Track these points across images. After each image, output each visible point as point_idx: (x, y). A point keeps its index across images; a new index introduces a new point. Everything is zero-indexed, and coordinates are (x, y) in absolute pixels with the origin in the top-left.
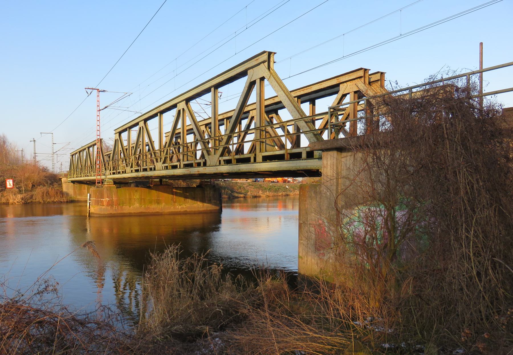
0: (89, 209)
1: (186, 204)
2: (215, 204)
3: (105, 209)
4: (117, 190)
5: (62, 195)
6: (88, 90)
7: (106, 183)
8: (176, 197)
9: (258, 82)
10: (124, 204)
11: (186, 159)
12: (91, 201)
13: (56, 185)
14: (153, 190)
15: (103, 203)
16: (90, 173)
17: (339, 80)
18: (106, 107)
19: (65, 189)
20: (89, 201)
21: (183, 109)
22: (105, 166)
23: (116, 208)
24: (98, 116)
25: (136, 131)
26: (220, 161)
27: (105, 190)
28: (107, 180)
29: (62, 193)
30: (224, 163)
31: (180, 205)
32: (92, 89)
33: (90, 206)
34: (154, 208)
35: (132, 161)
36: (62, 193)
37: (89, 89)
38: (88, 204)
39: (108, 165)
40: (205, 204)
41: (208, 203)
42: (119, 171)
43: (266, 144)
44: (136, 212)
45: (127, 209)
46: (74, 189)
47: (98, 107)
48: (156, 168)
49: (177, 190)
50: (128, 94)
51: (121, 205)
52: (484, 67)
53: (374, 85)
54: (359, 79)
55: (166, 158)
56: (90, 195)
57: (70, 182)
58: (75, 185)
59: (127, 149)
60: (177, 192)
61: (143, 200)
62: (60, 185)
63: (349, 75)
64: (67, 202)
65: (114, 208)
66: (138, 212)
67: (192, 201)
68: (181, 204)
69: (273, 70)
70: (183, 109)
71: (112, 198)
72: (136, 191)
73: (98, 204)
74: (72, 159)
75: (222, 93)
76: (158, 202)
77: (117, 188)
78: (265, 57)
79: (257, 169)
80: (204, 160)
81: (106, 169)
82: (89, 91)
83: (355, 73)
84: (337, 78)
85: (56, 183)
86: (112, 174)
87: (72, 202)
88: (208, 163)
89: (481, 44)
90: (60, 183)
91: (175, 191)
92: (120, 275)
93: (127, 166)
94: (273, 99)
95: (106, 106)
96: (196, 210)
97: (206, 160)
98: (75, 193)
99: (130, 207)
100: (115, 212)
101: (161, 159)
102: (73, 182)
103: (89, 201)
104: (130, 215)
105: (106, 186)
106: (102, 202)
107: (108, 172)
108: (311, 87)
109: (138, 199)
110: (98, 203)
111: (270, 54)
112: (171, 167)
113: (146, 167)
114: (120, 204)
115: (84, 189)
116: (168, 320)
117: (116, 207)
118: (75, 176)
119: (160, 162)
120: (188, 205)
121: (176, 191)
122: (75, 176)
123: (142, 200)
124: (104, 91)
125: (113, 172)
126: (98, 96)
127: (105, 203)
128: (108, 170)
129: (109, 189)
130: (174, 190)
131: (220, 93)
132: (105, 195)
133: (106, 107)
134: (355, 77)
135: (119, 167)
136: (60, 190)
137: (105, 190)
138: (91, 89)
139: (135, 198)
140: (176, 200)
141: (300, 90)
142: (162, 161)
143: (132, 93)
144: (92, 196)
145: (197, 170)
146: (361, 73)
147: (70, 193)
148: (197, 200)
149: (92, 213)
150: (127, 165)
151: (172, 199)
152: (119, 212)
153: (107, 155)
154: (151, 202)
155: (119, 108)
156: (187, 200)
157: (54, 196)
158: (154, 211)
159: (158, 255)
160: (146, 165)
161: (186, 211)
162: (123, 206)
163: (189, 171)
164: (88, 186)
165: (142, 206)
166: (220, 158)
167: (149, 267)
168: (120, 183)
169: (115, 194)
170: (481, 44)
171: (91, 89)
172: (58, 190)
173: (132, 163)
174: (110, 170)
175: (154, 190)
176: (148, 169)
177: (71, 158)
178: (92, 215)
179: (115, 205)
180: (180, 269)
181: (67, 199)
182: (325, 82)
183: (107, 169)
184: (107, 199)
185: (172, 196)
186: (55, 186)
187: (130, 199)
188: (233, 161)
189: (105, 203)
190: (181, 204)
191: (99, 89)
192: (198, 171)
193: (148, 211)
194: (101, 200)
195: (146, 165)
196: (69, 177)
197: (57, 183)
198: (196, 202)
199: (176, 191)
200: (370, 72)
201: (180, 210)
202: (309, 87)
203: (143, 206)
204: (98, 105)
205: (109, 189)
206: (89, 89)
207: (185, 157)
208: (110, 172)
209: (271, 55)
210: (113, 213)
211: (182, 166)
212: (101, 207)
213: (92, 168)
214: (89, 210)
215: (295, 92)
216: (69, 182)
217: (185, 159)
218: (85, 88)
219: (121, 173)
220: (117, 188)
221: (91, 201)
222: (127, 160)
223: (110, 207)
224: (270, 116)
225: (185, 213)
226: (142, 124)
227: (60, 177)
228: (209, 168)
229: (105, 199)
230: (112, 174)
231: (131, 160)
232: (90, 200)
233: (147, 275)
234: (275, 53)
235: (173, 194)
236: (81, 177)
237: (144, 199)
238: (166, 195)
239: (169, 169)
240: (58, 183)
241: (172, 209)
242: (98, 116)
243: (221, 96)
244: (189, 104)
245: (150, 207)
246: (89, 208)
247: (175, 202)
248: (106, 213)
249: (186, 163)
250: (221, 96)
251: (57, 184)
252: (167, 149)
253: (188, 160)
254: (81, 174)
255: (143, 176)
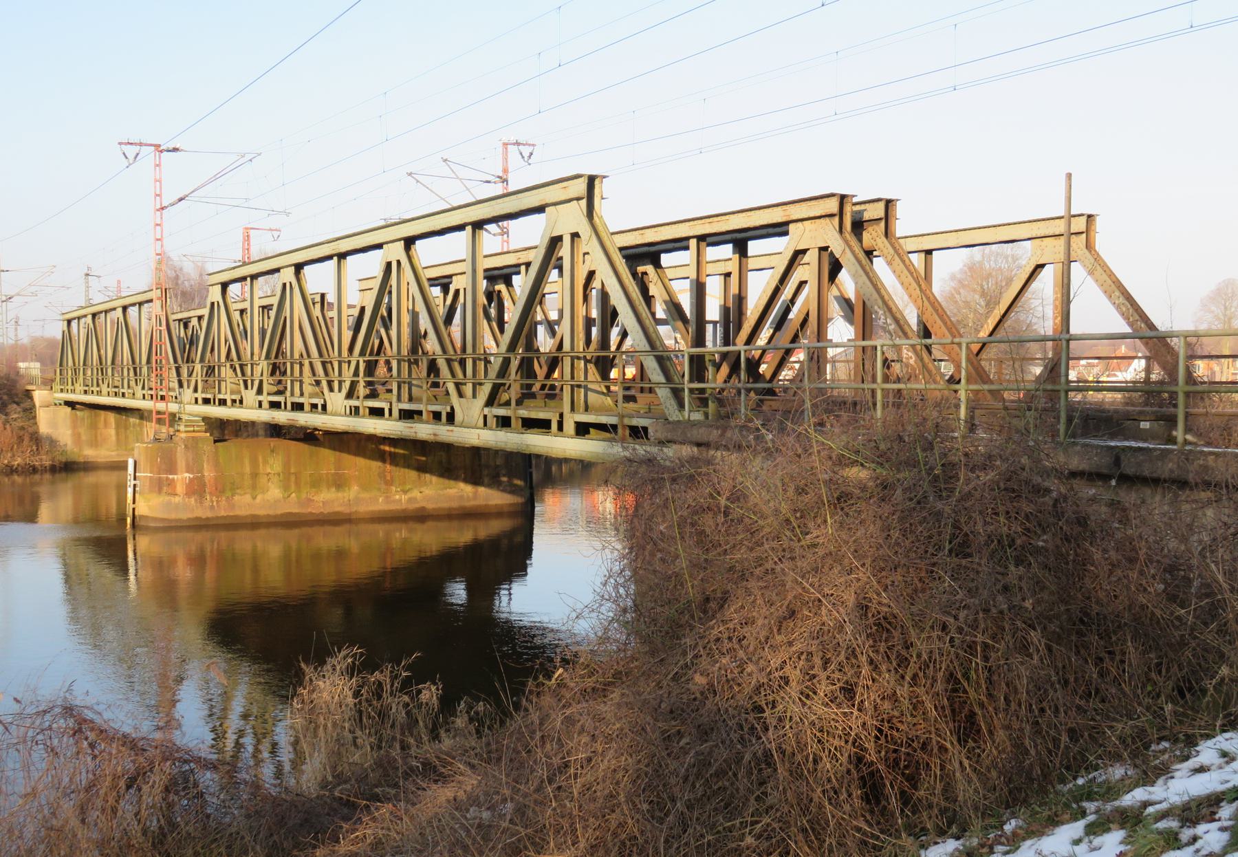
0: (132, 506)
1: (422, 489)
2: (513, 490)
3: (180, 505)
4: (216, 448)
5: (37, 446)
6: (127, 149)
7: (182, 428)
8: (394, 468)
9: (567, 240)
10: (238, 491)
11: (407, 395)
12: (137, 482)
13: (15, 412)
14: (322, 449)
15: (175, 487)
16: (129, 387)
17: (787, 213)
18: (181, 200)
19: (44, 428)
20: (133, 482)
21: (399, 262)
22: (179, 374)
23: (212, 502)
24: (157, 225)
25: (271, 230)
26: (485, 417)
27: (180, 449)
28: (185, 417)
29: (36, 439)
30: (497, 426)
31: (405, 492)
32: (141, 144)
33: (137, 495)
34: (327, 500)
35: (262, 375)
36: (37, 439)
37: (131, 144)
38: (130, 490)
39: (190, 375)
40: (482, 490)
41: (489, 486)
42: (221, 396)
43: (586, 389)
44: (271, 512)
45: (245, 504)
46: (74, 425)
47: (158, 198)
48: (329, 407)
49: (395, 447)
50: (248, 157)
51: (229, 494)
52: (1061, 241)
53: (870, 229)
54: (828, 220)
55: (353, 385)
56: (135, 463)
57: (62, 403)
58: (78, 413)
59: (242, 312)
60: (395, 453)
61: (293, 478)
62: (30, 412)
63: (809, 203)
64: (54, 469)
65: (207, 503)
66: (279, 512)
67: (441, 480)
68: (408, 487)
69: (601, 218)
70: (399, 262)
71: (201, 471)
72: (272, 451)
73: (160, 491)
74: (66, 332)
75: (533, 145)
76: (339, 483)
77: (215, 441)
78: (580, 187)
79: (564, 450)
80: (449, 409)
81: (181, 385)
82: (131, 151)
83: (821, 201)
84: (784, 207)
85: (15, 406)
86: (200, 401)
87: (68, 468)
88: (459, 417)
89: (1069, 176)
90: (27, 404)
91: (390, 452)
92: (226, 697)
93: (246, 388)
94: (641, 232)
95: (181, 196)
96: (455, 504)
97: (452, 408)
98: (77, 437)
99: (254, 498)
100: (209, 514)
101: (340, 383)
102: (71, 404)
103: (133, 482)
104: (254, 524)
105: (183, 435)
106: (171, 483)
107: (188, 394)
108: (727, 217)
109: (279, 474)
110: (160, 486)
111: (591, 180)
112: (367, 410)
113: (301, 400)
114: (223, 491)
115: (106, 424)
116: (330, 779)
117: (214, 498)
118: (79, 387)
119: (340, 390)
120: (428, 491)
121: (392, 450)
122: (79, 387)
123: (289, 480)
124: (175, 150)
125: (204, 396)
126: (157, 165)
127: (180, 489)
128: (188, 387)
129: (192, 444)
130: (387, 448)
131: (530, 145)
132: (181, 462)
133: (181, 200)
134: (818, 214)
135: (223, 384)
136: (31, 430)
137: (180, 449)
138: (135, 144)
139: (269, 470)
140: (392, 478)
141: (703, 221)
142: (345, 391)
143: (259, 154)
144: (141, 465)
145: (431, 432)
146: (832, 206)
147: (60, 438)
148: (456, 478)
149: (141, 517)
150: (245, 382)
151: (382, 475)
152: (223, 513)
153: (180, 320)
154: (316, 483)
155: (203, 200)
156: (428, 476)
157: (12, 449)
158: (327, 510)
159: (316, 668)
160: (302, 394)
161: (423, 509)
162: (233, 495)
163: (413, 430)
164: (118, 416)
165: (289, 496)
166: (486, 411)
167: (300, 690)
168: (223, 430)
169: (208, 461)
170: (1069, 176)
171: (135, 144)
172: (22, 428)
173: (261, 382)
174: (196, 390)
175: (324, 447)
176: (307, 407)
177: (66, 328)
178: (142, 523)
179: (211, 494)
180: (357, 694)
181: (53, 460)
182: (757, 212)
183: (185, 385)
184: (187, 475)
185: (380, 464)
186: (15, 416)
187: (255, 475)
188: (513, 421)
189: (180, 489)
190: (408, 487)
191: (159, 146)
192: (435, 435)
193: (309, 510)
194: (167, 479)
195: (302, 394)
196: (57, 387)
197: (18, 404)
198: (452, 483)
199: (392, 450)
200: (855, 200)
201: (404, 507)
202: (723, 218)
203: (294, 495)
204: (158, 192)
205: (192, 444)
206: (131, 144)
207: (405, 389)
208: (196, 395)
209: (597, 182)
210: (204, 517)
211: (396, 413)
212: (167, 498)
213: (135, 374)
214: (134, 509)
215: (692, 223)
216: (57, 402)
217: (405, 396)
218: (120, 144)
219: (229, 402)
220: (215, 441)
221: (137, 482)
222: (245, 367)
223: (196, 500)
224: (640, 269)
225: (420, 517)
226: (288, 275)
227: (29, 387)
228: (460, 429)
229: (180, 477)
230: (200, 401)
231: (258, 370)
232: (135, 479)
233: (296, 704)
234: (605, 177)
235: (384, 461)
236: (99, 393)
237: (295, 474)
238: (361, 462)
239: (363, 416)
240: (22, 405)
241: (380, 504)
242: (157, 225)
243: (531, 154)
244: (413, 249)
245: (315, 498)
246: (134, 503)
247: (389, 483)
248: (184, 515)
249: (406, 406)
250: (531, 154)
251: (19, 409)
252: (358, 361)
253: (411, 399)
254: (98, 385)
255: (291, 422)
